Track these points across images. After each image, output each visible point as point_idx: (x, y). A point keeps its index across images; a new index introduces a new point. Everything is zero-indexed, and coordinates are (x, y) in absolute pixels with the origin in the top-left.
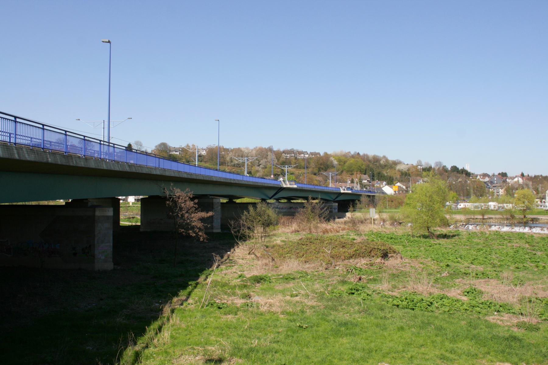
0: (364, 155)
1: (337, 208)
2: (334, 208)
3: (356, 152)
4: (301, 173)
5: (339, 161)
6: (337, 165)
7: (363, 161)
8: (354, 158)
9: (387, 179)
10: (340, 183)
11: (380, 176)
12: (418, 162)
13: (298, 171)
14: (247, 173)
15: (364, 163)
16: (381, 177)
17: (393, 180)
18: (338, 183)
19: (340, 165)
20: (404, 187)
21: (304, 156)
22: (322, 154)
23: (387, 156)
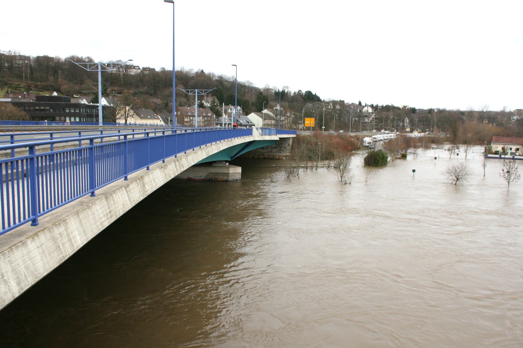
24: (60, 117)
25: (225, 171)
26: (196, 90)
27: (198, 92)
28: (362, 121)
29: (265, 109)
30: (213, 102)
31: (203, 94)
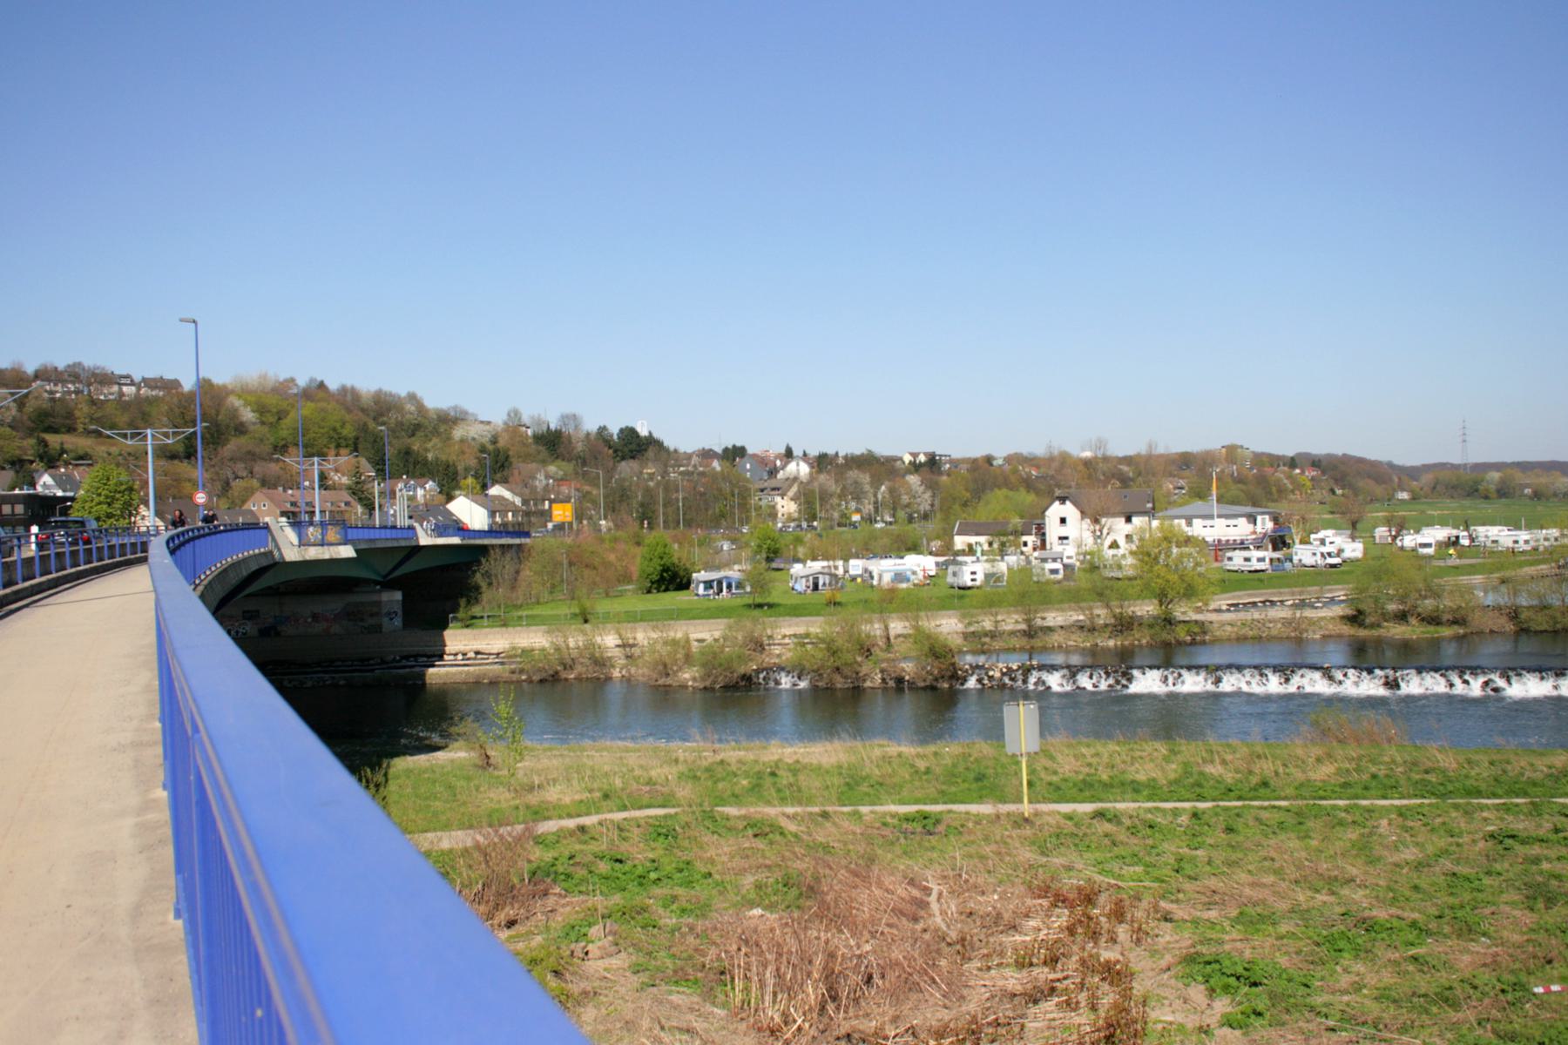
0: (344, 390)
1: (400, 613)
2: (389, 614)
3: (316, 380)
4: (120, 455)
5: (261, 410)
6: (254, 424)
7: (343, 412)
8: (312, 401)
9: (438, 471)
10: (290, 492)
11: (411, 460)
12: (509, 415)
13: (103, 448)
14: (931, 889)
15: (348, 417)
16: (416, 463)
17: (456, 473)
18: (281, 489)
19: (263, 423)
20: (518, 501)
21: (121, 394)
22: (188, 384)
23: (419, 394)
24: (13, 514)
25: (375, 598)
26: (149, 431)
27: (153, 436)
28: (598, 486)
29: (493, 485)
30: (358, 474)
31: (170, 442)
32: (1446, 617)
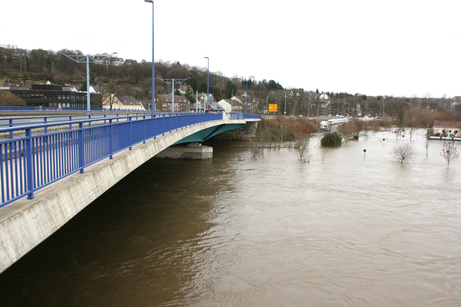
27: (174, 81)
29: (234, 96)
30: (188, 90)
31: (179, 83)
32: (106, 166)
